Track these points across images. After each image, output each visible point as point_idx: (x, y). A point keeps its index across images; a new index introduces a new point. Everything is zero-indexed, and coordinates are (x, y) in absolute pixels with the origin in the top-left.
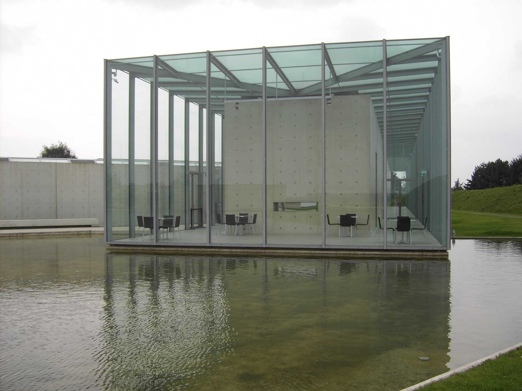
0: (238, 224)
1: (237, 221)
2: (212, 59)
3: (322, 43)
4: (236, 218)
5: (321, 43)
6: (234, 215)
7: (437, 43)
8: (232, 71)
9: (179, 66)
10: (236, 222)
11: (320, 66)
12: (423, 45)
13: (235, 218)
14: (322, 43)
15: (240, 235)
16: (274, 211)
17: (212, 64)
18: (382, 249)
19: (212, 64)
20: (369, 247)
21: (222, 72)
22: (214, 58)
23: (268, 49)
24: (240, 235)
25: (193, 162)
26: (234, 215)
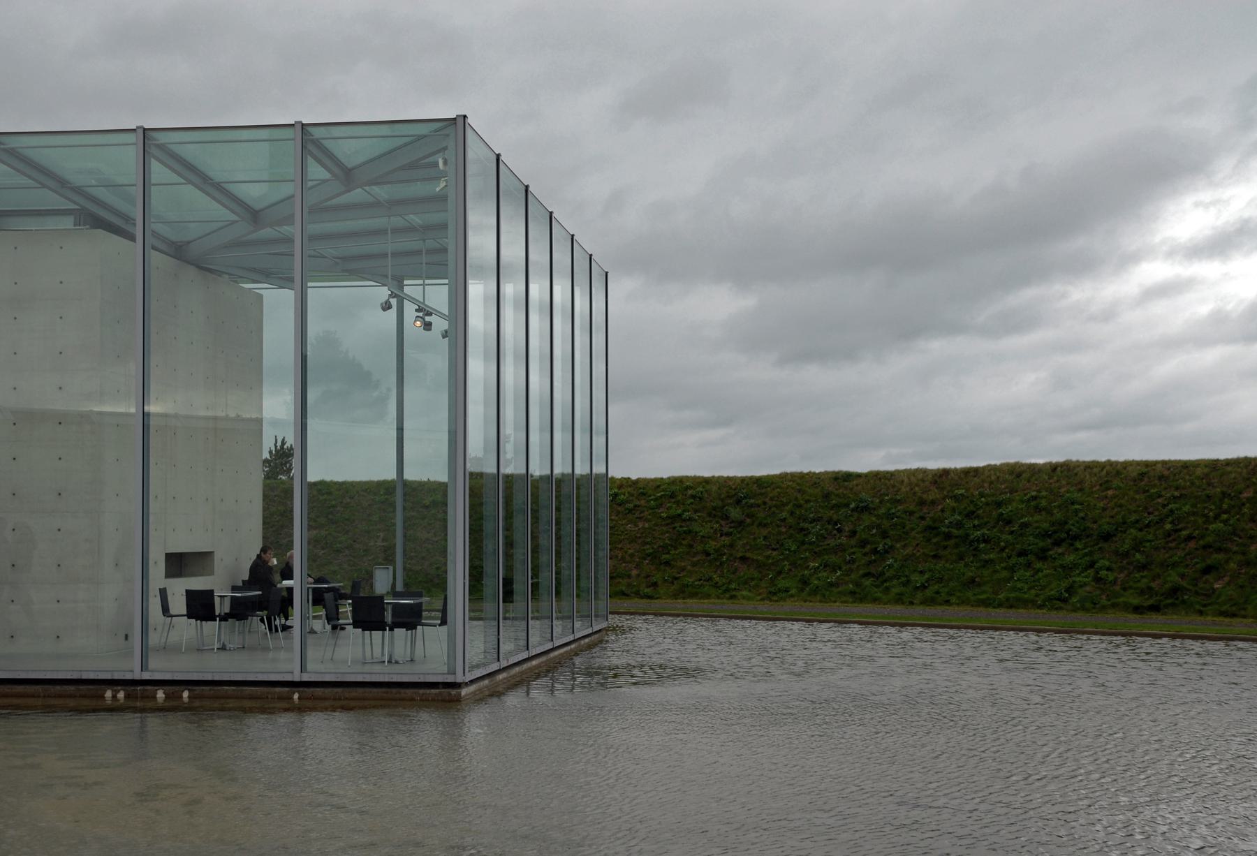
0: (224, 618)
1: (221, 607)
2: (310, 147)
3: (295, 122)
4: (217, 600)
5: (455, 116)
6: (212, 592)
7: (437, 133)
8: (227, 184)
9: (72, 165)
10: (217, 613)
11: (312, 178)
12: (412, 138)
13: (213, 599)
14: (295, 122)
15: (230, 650)
16: (165, 589)
17: (310, 161)
18: (453, 681)
19: (310, 161)
20: (421, 676)
21: (190, 187)
22: (317, 143)
23: (310, 129)
24: (230, 650)
25: (275, 423)
26: (212, 592)
